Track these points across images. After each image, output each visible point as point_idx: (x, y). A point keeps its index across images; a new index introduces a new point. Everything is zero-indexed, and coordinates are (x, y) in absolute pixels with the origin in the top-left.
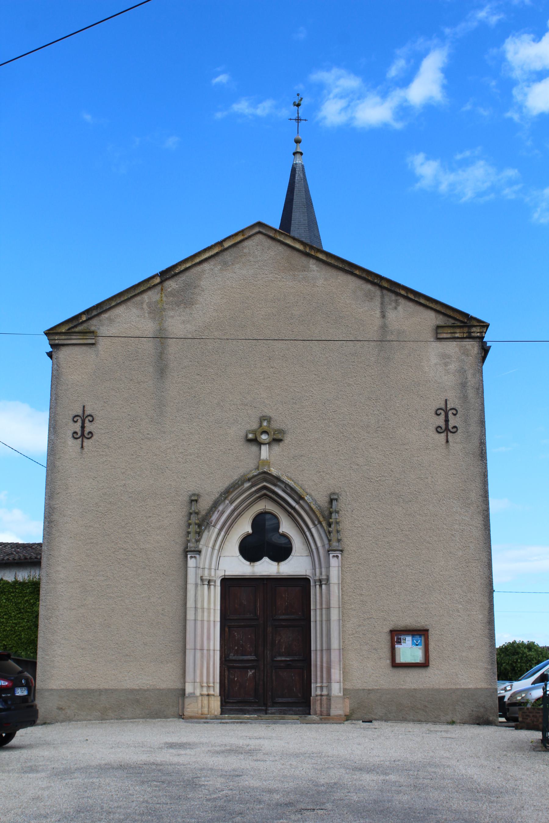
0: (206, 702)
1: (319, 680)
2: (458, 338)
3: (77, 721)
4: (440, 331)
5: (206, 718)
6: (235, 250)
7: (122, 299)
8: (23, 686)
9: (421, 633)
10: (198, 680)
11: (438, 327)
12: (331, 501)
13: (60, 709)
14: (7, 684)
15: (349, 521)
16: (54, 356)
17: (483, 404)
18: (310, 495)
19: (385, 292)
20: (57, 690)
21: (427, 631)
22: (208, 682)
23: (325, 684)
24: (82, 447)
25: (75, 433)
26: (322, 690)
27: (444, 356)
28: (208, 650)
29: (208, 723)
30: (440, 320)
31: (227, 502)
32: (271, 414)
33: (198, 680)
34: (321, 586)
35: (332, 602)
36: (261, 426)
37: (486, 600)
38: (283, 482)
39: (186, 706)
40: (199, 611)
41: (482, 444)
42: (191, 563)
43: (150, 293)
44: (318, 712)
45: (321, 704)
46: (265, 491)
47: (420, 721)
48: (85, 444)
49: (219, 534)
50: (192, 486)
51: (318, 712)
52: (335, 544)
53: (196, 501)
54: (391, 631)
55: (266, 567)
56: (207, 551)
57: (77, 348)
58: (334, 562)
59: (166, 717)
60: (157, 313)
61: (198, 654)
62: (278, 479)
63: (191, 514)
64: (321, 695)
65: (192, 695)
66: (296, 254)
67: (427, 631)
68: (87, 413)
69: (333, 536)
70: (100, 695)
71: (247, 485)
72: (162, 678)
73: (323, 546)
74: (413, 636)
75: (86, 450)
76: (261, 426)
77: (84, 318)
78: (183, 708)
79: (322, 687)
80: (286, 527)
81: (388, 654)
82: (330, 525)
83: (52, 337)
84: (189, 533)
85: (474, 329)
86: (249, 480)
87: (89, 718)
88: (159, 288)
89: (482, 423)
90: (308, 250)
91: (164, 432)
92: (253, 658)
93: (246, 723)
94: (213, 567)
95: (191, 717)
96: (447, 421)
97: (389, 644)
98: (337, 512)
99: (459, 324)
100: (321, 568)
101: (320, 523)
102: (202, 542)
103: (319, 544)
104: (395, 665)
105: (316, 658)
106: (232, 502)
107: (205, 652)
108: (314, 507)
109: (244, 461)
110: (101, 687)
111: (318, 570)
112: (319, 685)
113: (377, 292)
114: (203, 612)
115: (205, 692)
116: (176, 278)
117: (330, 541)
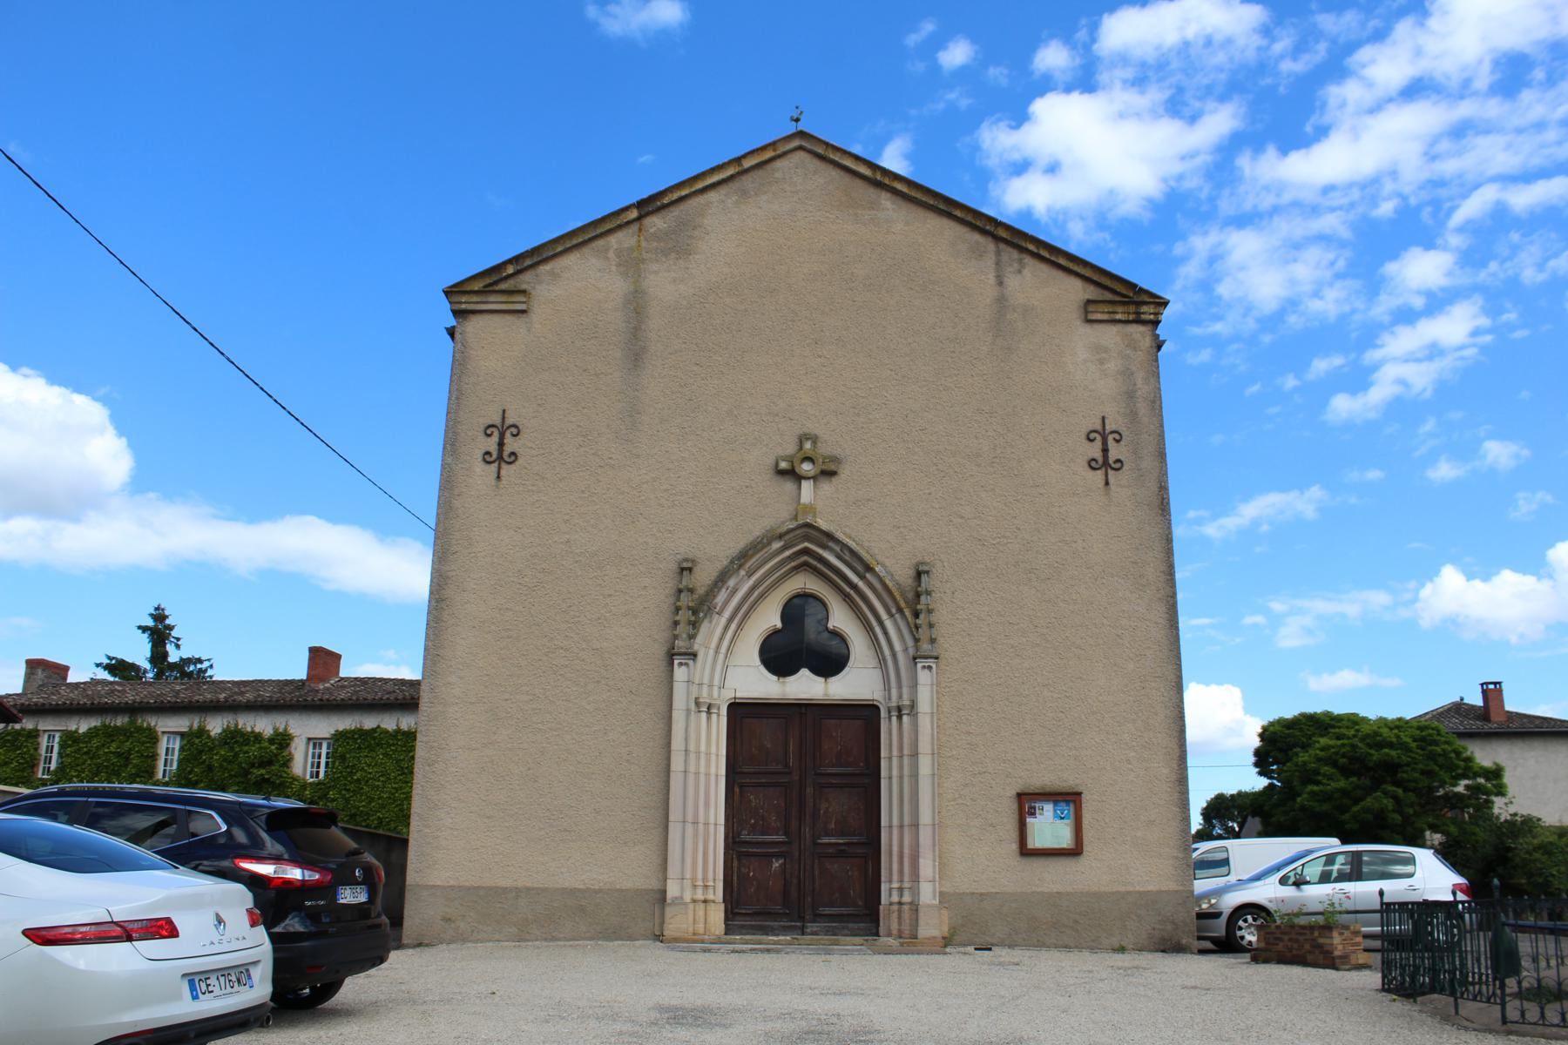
0: (701, 913)
1: (895, 877)
2: (1120, 321)
3: (477, 941)
4: (1090, 308)
5: (703, 942)
6: (759, 173)
7: (575, 242)
8: (358, 884)
9: (1069, 799)
10: (688, 876)
11: (1089, 302)
12: (919, 574)
13: (448, 920)
14: (317, 876)
15: (950, 607)
16: (458, 336)
17: (1162, 426)
18: (883, 565)
19: (1002, 246)
20: (444, 887)
21: (1080, 794)
22: (705, 879)
23: (906, 885)
24: (498, 477)
25: (488, 453)
26: (901, 896)
27: (1098, 349)
28: (707, 824)
29: (709, 951)
30: (1091, 292)
31: (742, 572)
32: (816, 432)
33: (688, 876)
34: (900, 717)
35: (920, 744)
36: (801, 448)
37: (1174, 745)
38: (837, 541)
39: (667, 920)
40: (692, 756)
41: (1163, 488)
42: (680, 673)
43: (620, 235)
44: (895, 932)
45: (900, 917)
46: (805, 558)
47: (1067, 947)
48: (503, 472)
49: (726, 628)
50: (683, 545)
51: (895, 932)
52: (925, 647)
53: (690, 569)
54: (1020, 796)
55: (805, 686)
56: (706, 655)
57: (496, 318)
58: (924, 677)
59: (631, 938)
60: (632, 265)
61: (690, 829)
62: (830, 536)
63: (680, 591)
64: (900, 903)
65: (679, 901)
66: (859, 182)
67: (1080, 794)
68: (509, 421)
69: (923, 633)
70: (517, 897)
71: (777, 545)
72: (626, 870)
73: (906, 650)
74: (1056, 803)
75: (504, 481)
76: (801, 448)
77: (510, 270)
78: (662, 923)
79: (901, 890)
80: (840, 619)
81: (1014, 835)
82: (916, 615)
83: (456, 298)
84: (676, 623)
85: (1145, 309)
86: (780, 537)
87: (497, 936)
88: (635, 227)
89: (1161, 455)
90: (879, 177)
91: (638, 456)
92: (782, 838)
93: (778, 951)
94: (716, 682)
95: (676, 940)
96: (1105, 451)
97: (1016, 816)
98: (928, 593)
99: (1118, 298)
100: (900, 687)
101: (900, 610)
102: (699, 639)
103: (898, 646)
104: (1025, 852)
105: (889, 839)
106: (750, 575)
107: (701, 827)
108: (890, 584)
109: (773, 508)
110: (520, 884)
111: (894, 692)
112: (895, 885)
113: (989, 245)
114: (698, 758)
115: (700, 896)
116: (664, 212)
117: (917, 640)
